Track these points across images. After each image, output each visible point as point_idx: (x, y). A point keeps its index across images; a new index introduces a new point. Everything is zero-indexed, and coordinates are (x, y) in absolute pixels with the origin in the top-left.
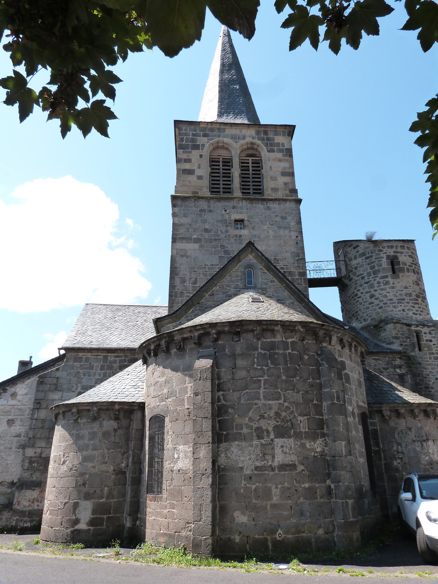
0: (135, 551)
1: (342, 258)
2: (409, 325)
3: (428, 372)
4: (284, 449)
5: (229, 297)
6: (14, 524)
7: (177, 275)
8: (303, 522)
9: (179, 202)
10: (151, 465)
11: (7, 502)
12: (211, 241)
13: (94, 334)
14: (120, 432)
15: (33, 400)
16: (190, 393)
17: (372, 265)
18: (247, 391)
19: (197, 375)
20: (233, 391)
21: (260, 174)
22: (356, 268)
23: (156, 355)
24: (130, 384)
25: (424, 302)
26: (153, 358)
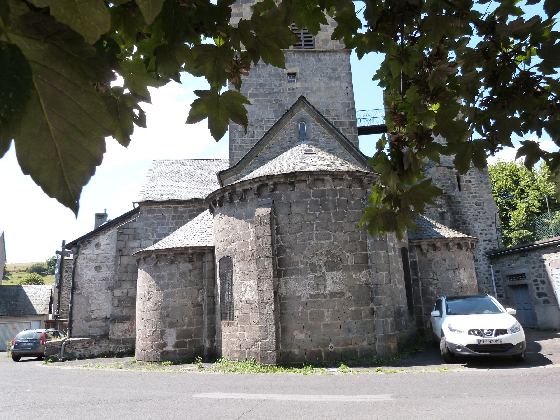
0: (214, 365)
4: (334, 280)
5: (285, 149)
6: (111, 350)
8: (350, 336)
10: (223, 298)
11: (103, 333)
12: (265, 95)
13: (164, 188)
14: (194, 272)
15: (115, 249)
16: (253, 237)
19: (258, 222)
20: (290, 234)
23: (221, 205)
26: (219, 208)
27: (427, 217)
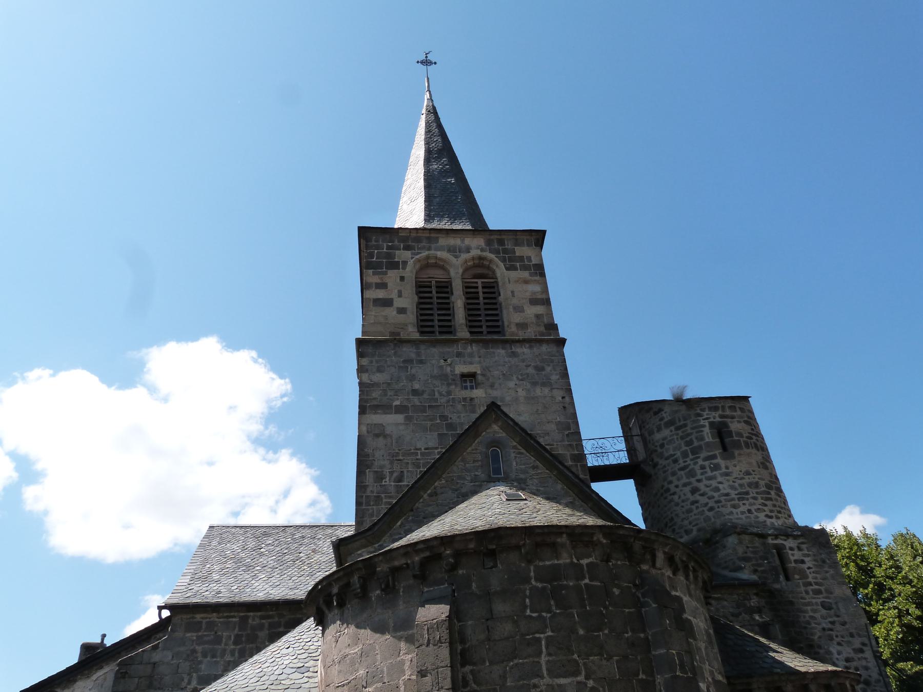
1: (636, 431)
2: (763, 536)
3: (808, 618)
5: (464, 497)
7: (368, 467)
9: (370, 350)
12: (423, 409)
16: (409, 673)
17: (688, 439)
18: (516, 661)
19: (422, 636)
20: (491, 663)
21: (495, 304)
22: (662, 446)
24: (291, 665)
25: (780, 496)
27: (749, 631)
